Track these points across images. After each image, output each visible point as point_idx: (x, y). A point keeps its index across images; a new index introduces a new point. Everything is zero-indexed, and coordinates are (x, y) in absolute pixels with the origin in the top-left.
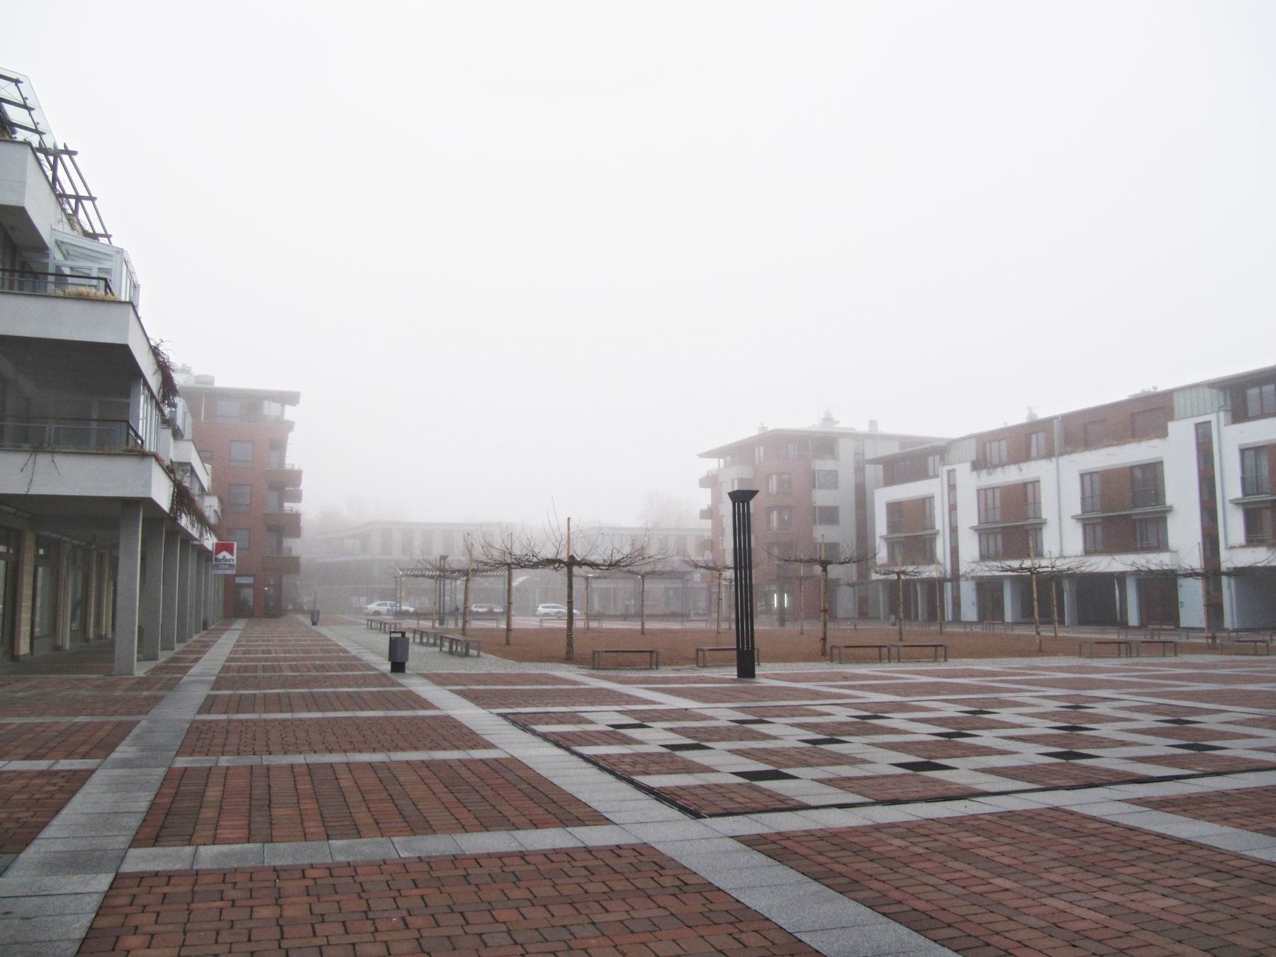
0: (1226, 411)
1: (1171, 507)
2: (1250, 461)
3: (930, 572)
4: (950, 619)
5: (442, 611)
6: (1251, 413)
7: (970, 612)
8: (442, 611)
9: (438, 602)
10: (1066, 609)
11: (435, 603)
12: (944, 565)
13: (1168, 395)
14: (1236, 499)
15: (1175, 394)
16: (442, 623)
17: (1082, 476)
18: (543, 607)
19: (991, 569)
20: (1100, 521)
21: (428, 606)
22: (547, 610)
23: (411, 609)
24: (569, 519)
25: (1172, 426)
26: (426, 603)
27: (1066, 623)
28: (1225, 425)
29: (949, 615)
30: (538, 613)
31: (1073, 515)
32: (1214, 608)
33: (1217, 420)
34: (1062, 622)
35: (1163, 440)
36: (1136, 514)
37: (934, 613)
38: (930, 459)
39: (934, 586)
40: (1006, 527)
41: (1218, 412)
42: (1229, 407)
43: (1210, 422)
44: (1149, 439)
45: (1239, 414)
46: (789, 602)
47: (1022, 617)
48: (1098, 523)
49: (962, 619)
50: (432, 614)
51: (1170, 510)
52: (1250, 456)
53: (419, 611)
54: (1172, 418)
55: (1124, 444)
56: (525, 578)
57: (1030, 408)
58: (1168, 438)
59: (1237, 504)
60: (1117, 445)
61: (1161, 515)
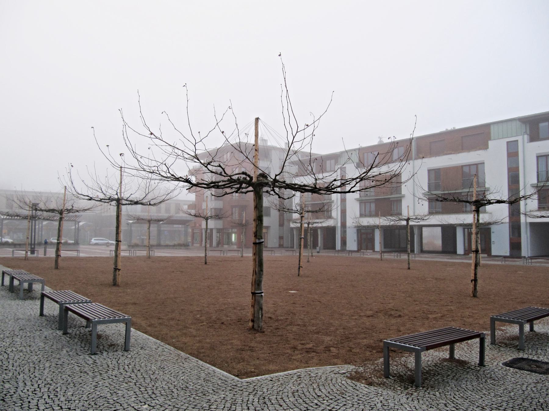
0: (527, 134)
1: (404, 195)
2: (433, 176)
3: (329, 223)
4: (339, 249)
5: (33, 243)
6: (541, 136)
7: (352, 244)
8: (33, 243)
9: (30, 237)
10: (415, 243)
11: (28, 238)
12: (337, 219)
13: (487, 126)
14: (357, 199)
15: (492, 127)
16: (33, 252)
17: (429, 171)
18: (94, 240)
19: (367, 221)
20: (374, 201)
21: (21, 238)
22: (97, 242)
23: (10, 241)
24: (257, 119)
25: (490, 143)
26: (21, 237)
27: (415, 252)
28: (527, 143)
29: (338, 246)
30: (91, 243)
31: (356, 198)
32: (515, 246)
33: (522, 139)
34: (412, 251)
35: (486, 151)
36: (392, 198)
37: (330, 244)
38: (328, 162)
39: (330, 232)
40: (314, 204)
41: (524, 135)
42: (528, 132)
43: (517, 141)
44: (476, 151)
45: (534, 137)
46: (232, 236)
47: (385, 248)
48: (373, 202)
49: (347, 249)
50: (25, 244)
51: (404, 196)
52: (543, 161)
53: (16, 242)
54: (490, 140)
55: (459, 153)
56: (84, 223)
57: (380, 138)
58: (488, 150)
59: (357, 200)
60: (454, 153)
61: (399, 199)
